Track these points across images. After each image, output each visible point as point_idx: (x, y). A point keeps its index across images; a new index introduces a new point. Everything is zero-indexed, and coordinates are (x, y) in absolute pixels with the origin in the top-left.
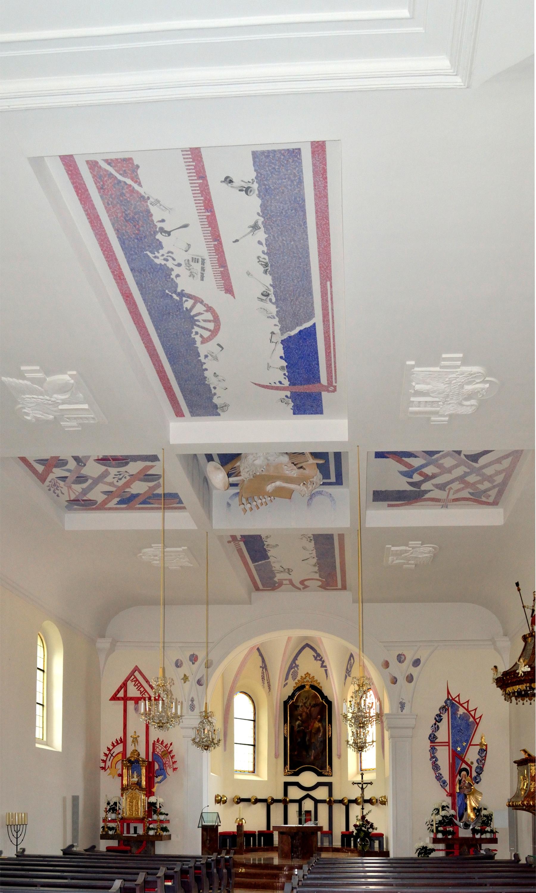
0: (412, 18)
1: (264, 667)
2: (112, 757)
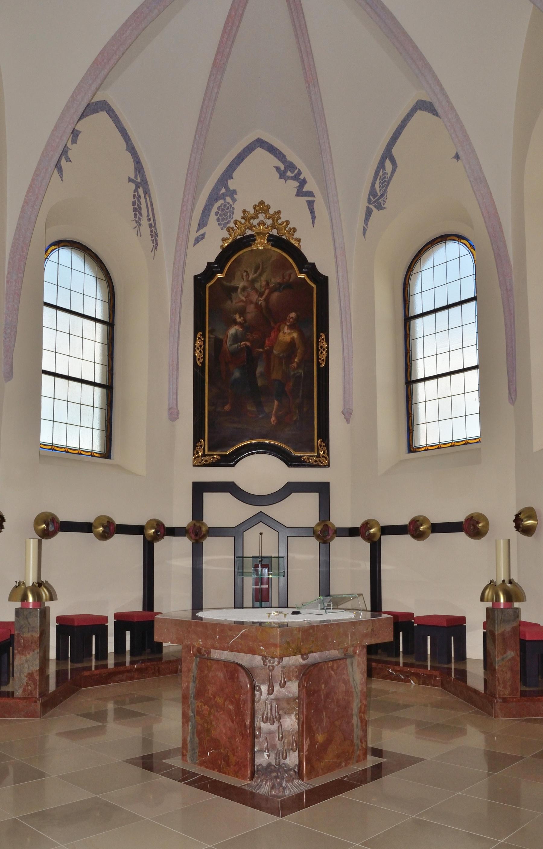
1: (140, 182)
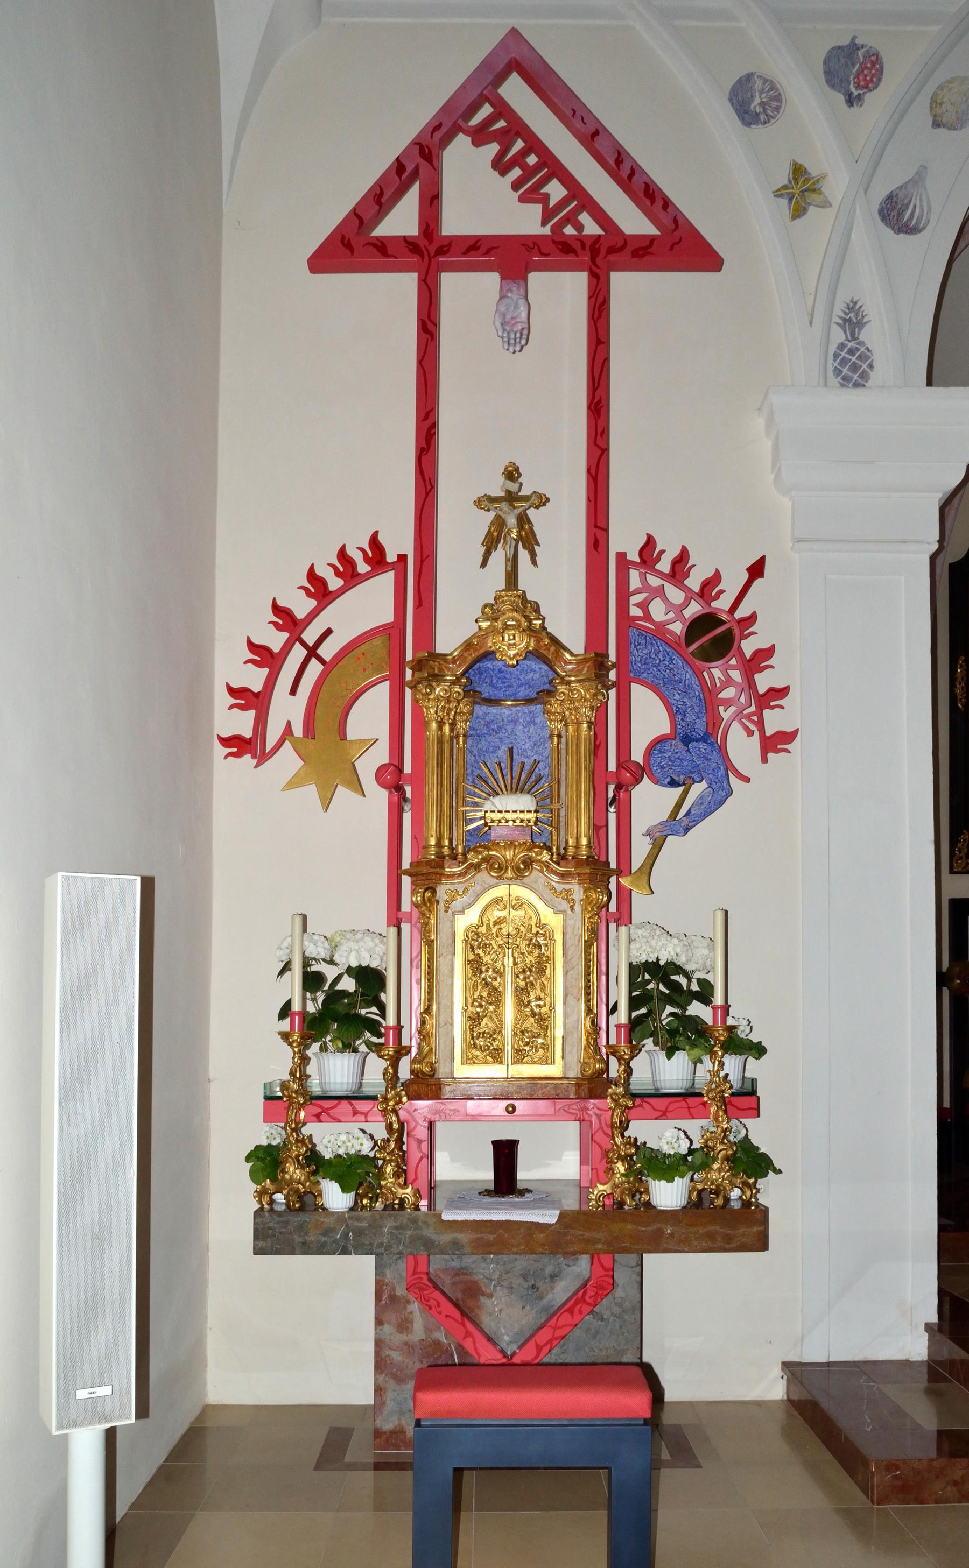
0: (515, 66)
2: (315, 668)
